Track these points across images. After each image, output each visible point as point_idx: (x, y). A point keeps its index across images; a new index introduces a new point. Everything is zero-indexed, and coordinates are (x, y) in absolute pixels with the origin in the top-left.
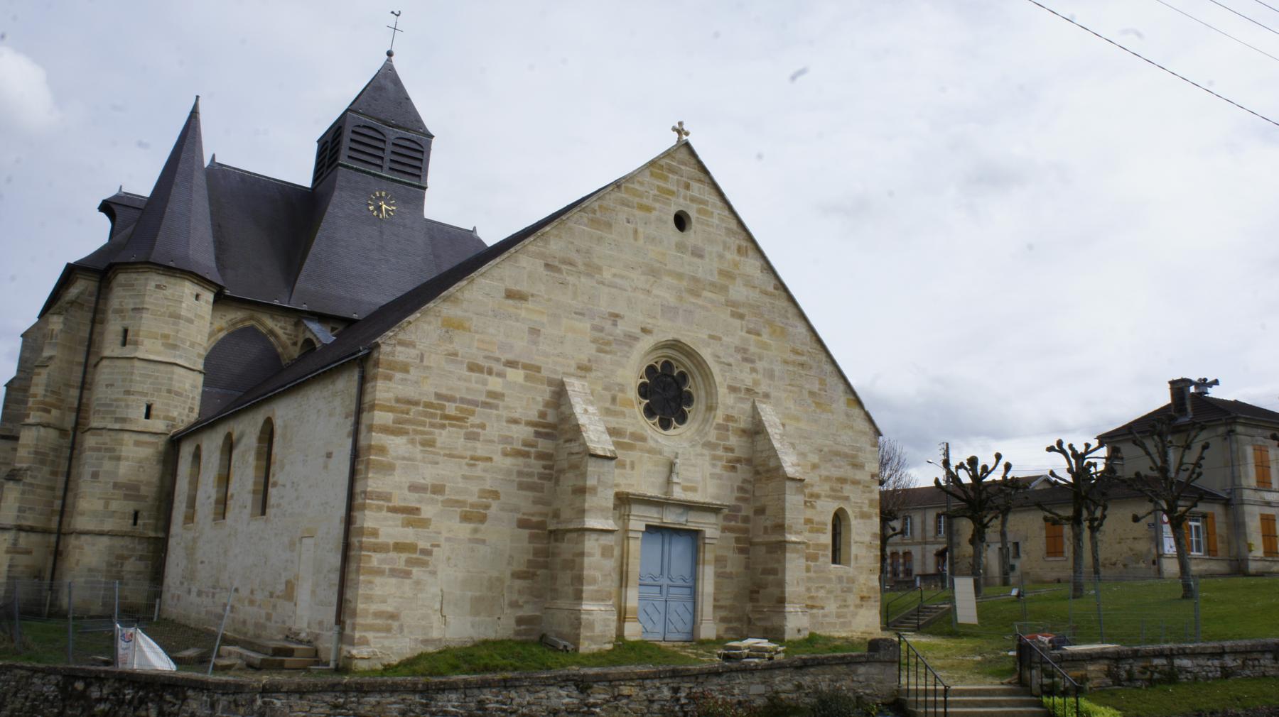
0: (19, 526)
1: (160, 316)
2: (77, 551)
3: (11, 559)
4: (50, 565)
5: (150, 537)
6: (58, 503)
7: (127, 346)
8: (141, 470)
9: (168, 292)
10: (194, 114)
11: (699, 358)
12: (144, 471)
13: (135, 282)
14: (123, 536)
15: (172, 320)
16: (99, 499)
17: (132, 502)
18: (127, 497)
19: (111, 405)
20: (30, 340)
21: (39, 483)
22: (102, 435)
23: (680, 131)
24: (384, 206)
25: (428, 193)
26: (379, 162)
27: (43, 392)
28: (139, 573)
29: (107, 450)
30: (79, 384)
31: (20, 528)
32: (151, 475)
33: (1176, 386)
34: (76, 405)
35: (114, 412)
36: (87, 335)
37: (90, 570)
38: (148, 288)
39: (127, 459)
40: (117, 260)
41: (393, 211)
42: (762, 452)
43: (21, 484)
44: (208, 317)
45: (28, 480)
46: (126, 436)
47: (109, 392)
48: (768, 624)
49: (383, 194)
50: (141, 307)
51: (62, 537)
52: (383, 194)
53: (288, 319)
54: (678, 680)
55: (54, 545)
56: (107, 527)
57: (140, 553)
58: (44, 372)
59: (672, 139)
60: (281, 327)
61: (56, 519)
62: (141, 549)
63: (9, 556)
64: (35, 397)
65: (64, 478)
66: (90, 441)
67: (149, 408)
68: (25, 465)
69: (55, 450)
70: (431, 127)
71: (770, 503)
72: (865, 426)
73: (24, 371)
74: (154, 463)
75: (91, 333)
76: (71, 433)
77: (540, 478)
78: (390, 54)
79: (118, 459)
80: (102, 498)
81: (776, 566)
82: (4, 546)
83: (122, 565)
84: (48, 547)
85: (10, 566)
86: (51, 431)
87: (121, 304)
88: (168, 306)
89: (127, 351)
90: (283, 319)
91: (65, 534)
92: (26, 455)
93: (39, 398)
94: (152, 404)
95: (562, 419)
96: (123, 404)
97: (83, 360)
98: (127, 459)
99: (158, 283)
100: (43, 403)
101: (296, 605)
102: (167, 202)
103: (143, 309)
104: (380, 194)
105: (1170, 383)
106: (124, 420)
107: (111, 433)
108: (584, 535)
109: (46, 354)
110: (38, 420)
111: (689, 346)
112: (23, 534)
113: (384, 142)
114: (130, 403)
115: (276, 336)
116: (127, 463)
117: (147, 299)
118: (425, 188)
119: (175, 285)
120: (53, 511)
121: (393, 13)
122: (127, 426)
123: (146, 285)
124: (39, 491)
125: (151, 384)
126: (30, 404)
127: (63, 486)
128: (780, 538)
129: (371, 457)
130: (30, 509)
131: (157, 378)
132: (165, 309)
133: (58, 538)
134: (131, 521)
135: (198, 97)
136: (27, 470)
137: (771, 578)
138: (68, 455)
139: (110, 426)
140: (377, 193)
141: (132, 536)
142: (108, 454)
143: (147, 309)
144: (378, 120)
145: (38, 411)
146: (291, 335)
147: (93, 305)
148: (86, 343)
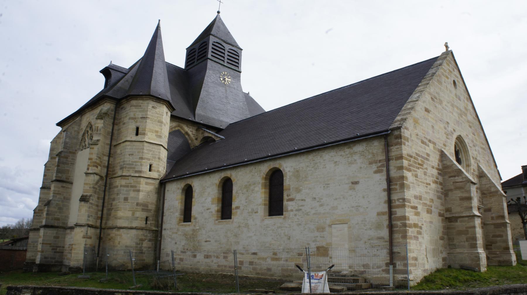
1: (154, 121)
2: (119, 237)
3: (86, 241)
5: (154, 230)
6: (100, 213)
7: (139, 136)
8: (149, 197)
9: (157, 110)
10: (158, 28)
11: (465, 144)
12: (150, 197)
13: (142, 105)
15: (159, 124)
16: (129, 211)
17: (145, 213)
18: (143, 210)
20: (69, 133)
22: (128, 179)
23: (447, 47)
24: (227, 79)
25: (242, 74)
26: (223, 59)
28: (149, 248)
29: (132, 186)
30: (108, 154)
31: (89, 226)
32: (153, 199)
33: (524, 168)
35: (134, 168)
36: (111, 130)
37: (126, 246)
38: (149, 107)
39: (142, 191)
40: (132, 93)
41: (230, 81)
42: (485, 185)
43: (89, 203)
44: (169, 124)
47: (131, 158)
48: (501, 259)
49: (226, 73)
50: (146, 117)
51: (102, 230)
52: (226, 73)
53: (193, 127)
54: (442, 286)
55: (99, 234)
56: (134, 225)
57: (149, 238)
59: (444, 50)
60: (191, 131)
61: (99, 221)
62: (149, 235)
63: (85, 239)
64: (92, 160)
65: (102, 201)
66: (119, 182)
67: (151, 166)
70: (241, 46)
71: (494, 207)
72: (498, 177)
73: (66, 148)
74: (154, 193)
75: (113, 130)
76: (105, 178)
77: (441, 194)
78: (218, 12)
79: (139, 191)
80: (131, 211)
81: (502, 233)
82: (82, 235)
83: (142, 243)
84: (96, 235)
87: (134, 115)
89: (139, 138)
90: (191, 127)
91: (104, 229)
92: (88, 188)
94: (152, 164)
95: (445, 167)
96: (139, 164)
97: (109, 143)
98: (142, 191)
99: (153, 106)
100: (96, 162)
101: (331, 258)
102: (153, 67)
103: (147, 117)
104: (225, 73)
105: (522, 167)
106: (140, 172)
107: (133, 178)
108: (474, 218)
109: (95, 138)
110: (94, 171)
112: (89, 228)
113: (224, 50)
114: (143, 164)
115: (189, 135)
117: (148, 113)
118: (240, 72)
119: (160, 107)
123: (148, 106)
125: (151, 154)
127: (102, 205)
128: (504, 221)
129: (404, 182)
134: (145, 222)
137: (499, 239)
138: (104, 189)
139: (132, 175)
140: (224, 73)
142: (132, 189)
143: (149, 118)
144: (222, 40)
145: (93, 166)
146: (195, 135)
147: (113, 116)
148: (111, 134)
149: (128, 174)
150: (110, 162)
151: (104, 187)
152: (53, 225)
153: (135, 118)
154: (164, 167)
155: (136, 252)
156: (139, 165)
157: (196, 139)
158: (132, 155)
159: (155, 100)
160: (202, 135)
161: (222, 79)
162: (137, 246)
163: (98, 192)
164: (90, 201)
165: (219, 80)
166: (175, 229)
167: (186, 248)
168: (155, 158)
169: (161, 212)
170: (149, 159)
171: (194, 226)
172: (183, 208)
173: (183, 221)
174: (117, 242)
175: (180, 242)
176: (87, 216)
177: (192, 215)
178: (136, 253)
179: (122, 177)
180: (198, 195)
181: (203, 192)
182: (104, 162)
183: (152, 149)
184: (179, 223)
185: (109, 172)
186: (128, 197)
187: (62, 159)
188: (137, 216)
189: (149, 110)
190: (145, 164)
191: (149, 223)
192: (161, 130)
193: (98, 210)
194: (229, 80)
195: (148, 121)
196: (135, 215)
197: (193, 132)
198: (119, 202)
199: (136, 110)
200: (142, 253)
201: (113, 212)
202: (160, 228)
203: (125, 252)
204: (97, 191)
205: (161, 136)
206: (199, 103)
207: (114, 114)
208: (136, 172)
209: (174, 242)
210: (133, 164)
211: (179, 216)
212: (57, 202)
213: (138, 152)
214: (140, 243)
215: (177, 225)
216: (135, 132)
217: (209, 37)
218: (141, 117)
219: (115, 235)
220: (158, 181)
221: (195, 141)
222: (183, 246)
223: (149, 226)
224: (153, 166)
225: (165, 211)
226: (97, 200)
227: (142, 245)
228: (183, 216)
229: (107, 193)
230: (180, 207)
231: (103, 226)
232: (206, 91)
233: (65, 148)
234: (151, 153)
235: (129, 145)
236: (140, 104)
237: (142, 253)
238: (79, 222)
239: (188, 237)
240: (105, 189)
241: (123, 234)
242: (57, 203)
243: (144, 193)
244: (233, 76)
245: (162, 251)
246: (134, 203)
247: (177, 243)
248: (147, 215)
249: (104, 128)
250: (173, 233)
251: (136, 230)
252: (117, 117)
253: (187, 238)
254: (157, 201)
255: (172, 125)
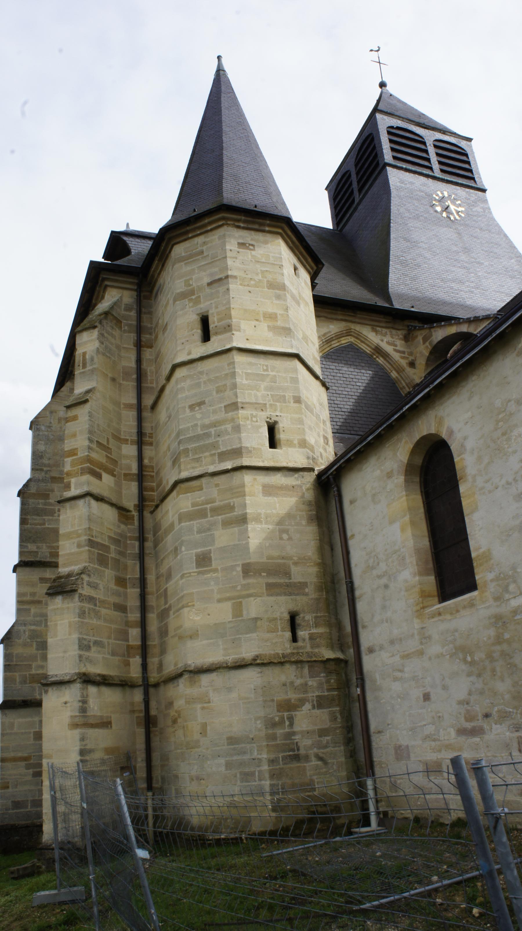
0: (84, 674)
1: (256, 286)
3: (82, 739)
4: (140, 744)
5: (329, 660)
6: (135, 633)
8: (285, 536)
12: (290, 539)
14: (282, 663)
16: (219, 601)
17: (282, 598)
19: (207, 435)
20: (43, 428)
21: (102, 597)
22: (201, 489)
24: (452, 208)
27: (87, 443)
28: (322, 733)
29: (216, 511)
30: (135, 438)
34: (134, 469)
35: (215, 446)
36: (133, 364)
37: (232, 740)
39: (257, 519)
41: (462, 212)
45: (86, 591)
46: (248, 478)
47: (198, 416)
51: (152, 690)
53: (394, 332)
55: (142, 707)
58: (82, 412)
60: (388, 343)
61: (136, 661)
63: (77, 733)
64: (76, 454)
65: (138, 590)
67: (272, 429)
68: (76, 568)
69: (116, 542)
73: (42, 470)
74: (304, 522)
75: (139, 361)
76: (135, 514)
83: (291, 719)
84: (133, 711)
85: (82, 752)
86: (106, 507)
88: (263, 272)
89: (214, 346)
90: (388, 331)
91: (156, 685)
92: (74, 549)
93: (81, 454)
94: (276, 423)
96: (229, 427)
97: (134, 401)
98: (257, 519)
99: (241, 241)
102: (222, 149)
104: (442, 193)
106: (238, 452)
107: (217, 480)
110: (85, 489)
111: (349, 609)
112: (92, 690)
115: (385, 355)
116: (258, 527)
117: (230, 262)
119: (266, 243)
120: (129, 647)
121: (371, 50)
122: (246, 462)
123: (224, 244)
124: (104, 611)
125: (266, 389)
126: (67, 468)
127: (138, 603)
130: (96, 643)
131: (274, 380)
132: (260, 277)
133: (146, 694)
134: (288, 634)
135: (219, 57)
136: (83, 572)
139: (212, 469)
141: (296, 662)
143: (235, 277)
145: (82, 474)
146: (403, 352)
147: (134, 323)
148: (135, 376)
149: (196, 473)
150: (146, 461)
151: (137, 544)
152: (29, 698)
153: (192, 292)
154: (325, 438)
155: (272, 756)
156: (230, 430)
157: (412, 364)
158: (201, 404)
159: (245, 222)
160: (427, 344)
161: (439, 209)
162: (270, 731)
163: (117, 561)
164: (80, 591)
165: (432, 211)
166: (413, 635)
167: (479, 709)
168: (282, 399)
169: (344, 589)
170: (263, 407)
171: (497, 599)
172: (426, 542)
173: (436, 599)
174: (194, 727)
175: (445, 688)
176: (76, 647)
177: (473, 555)
178: (272, 762)
179: (178, 488)
180: (480, 459)
181: (504, 434)
182: (124, 462)
183: (267, 370)
184: (423, 608)
185: (145, 493)
186: (210, 552)
187: (31, 501)
188: (253, 614)
189: (229, 254)
190: (248, 422)
191: (307, 637)
192: (287, 309)
193: (128, 624)
194: (460, 209)
195: (232, 286)
196: (245, 612)
197: (396, 346)
198: (182, 577)
199: (189, 268)
200: (297, 758)
201: (172, 622)
202: (352, 650)
203: (229, 765)
204: (113, 555)
205: (289, 329)
206: (391, 271)
207: (135, 318)
208: (223, 456)
209: (417, 693)
210: (207, 435)
211: (417, 578)
212: (33, 627)
213: (219, 391)
214: (282, 718)
215: (416, 621)
216: (212, 352)
217: (376, 116)
218: (209, 281)
219: (188, 702)
220: (310, 478)
221: (409, 371)
222: (460, 703)
223: (308, 649)
224: (281, 426)
225: (357, 581)
226: (113, 586)
227: (291, 725)
228: (432, 579)
229: (150, 563)
230: (411, 543)
231: (154, 676)
232: (405, 239)
233: (37, 470)
234: (263, 385)
235: (184, 378)
236: (200, 248)
237: (297, 758)
238: (56, 673)
239: (479, 656)
240: (142, 548)
241: (212, 695)
242: (33, 630)
243: (264, 526)
244: (469, 201)
245: (375, 740)
246: (233, 568)
247: (432, 696)
248: (292, 607)
249: (104, 354)
250: (406, 656)
251: (258, 669)
252: (145, 323)
253: (472, 663)
254: (321, 550)
255: (325, 330)
